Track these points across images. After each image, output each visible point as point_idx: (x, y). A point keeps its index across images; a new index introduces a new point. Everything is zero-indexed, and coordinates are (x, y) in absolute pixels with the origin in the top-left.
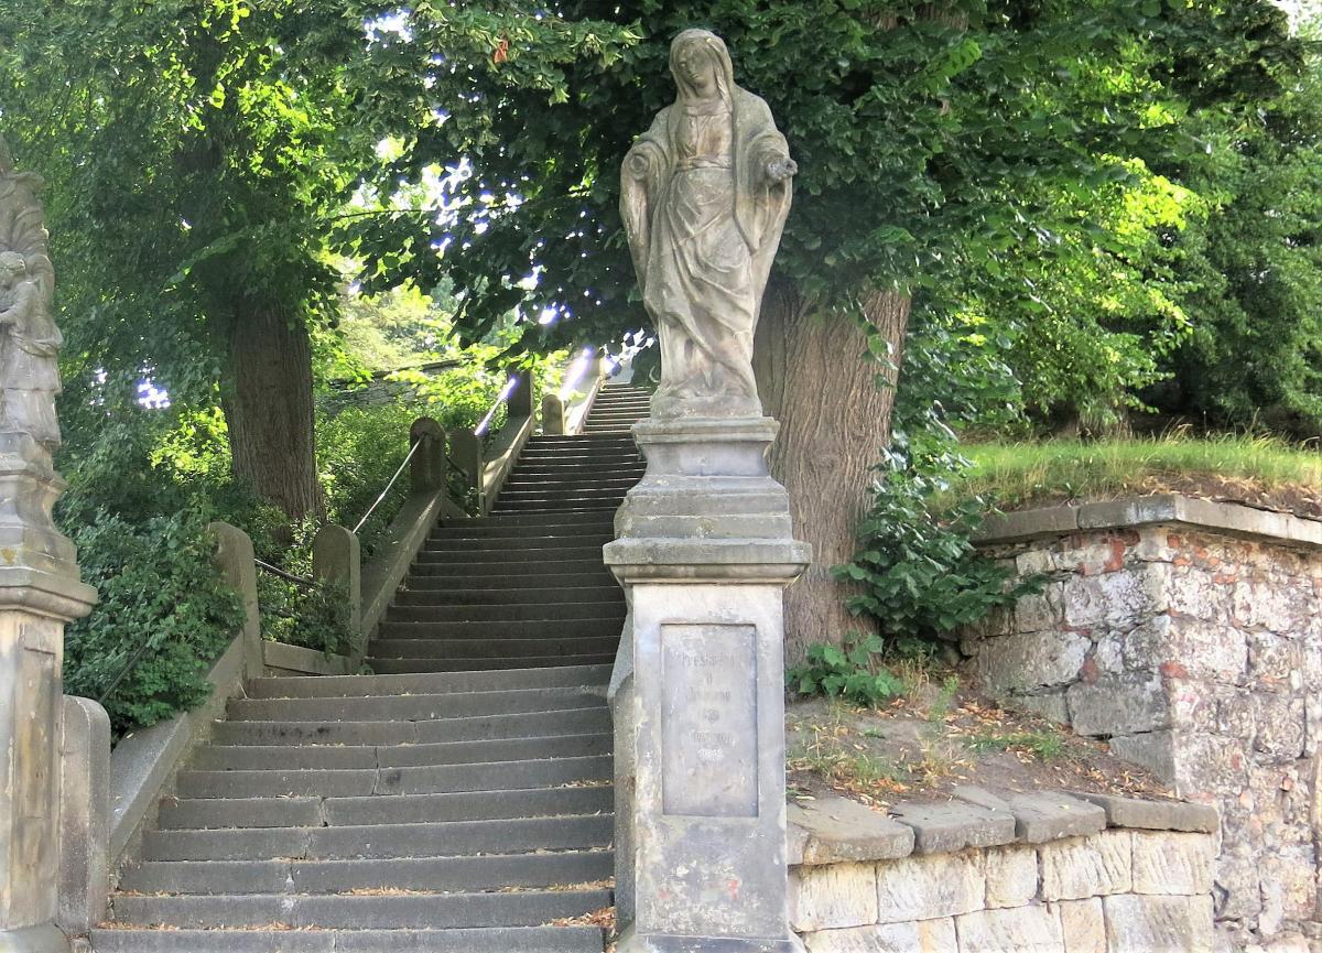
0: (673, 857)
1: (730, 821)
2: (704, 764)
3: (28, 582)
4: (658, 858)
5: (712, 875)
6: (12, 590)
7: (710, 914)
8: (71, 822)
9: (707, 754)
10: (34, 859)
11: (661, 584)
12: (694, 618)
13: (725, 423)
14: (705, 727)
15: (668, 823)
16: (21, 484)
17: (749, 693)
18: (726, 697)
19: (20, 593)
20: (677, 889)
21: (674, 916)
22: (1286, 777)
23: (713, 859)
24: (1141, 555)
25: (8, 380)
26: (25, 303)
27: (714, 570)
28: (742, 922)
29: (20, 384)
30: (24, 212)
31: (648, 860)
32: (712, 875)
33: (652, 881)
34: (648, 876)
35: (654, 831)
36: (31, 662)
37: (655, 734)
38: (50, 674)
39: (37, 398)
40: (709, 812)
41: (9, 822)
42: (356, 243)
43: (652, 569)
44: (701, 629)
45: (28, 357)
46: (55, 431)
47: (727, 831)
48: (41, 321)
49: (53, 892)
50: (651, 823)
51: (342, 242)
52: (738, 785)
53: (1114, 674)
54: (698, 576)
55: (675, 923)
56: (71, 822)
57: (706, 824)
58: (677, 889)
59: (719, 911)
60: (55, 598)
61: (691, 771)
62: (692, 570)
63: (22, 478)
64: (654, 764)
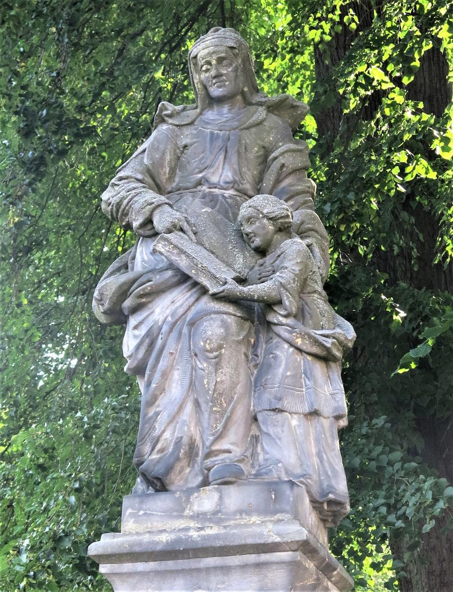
16: (295, 567)
25: (267, 396)
26: (297, 269)
29: (286, 404)
30: (280, 150)
39: (312, 428)
42: (387, 16)
45: (299, 357)
48: (320, 303)
63: (299, 556)
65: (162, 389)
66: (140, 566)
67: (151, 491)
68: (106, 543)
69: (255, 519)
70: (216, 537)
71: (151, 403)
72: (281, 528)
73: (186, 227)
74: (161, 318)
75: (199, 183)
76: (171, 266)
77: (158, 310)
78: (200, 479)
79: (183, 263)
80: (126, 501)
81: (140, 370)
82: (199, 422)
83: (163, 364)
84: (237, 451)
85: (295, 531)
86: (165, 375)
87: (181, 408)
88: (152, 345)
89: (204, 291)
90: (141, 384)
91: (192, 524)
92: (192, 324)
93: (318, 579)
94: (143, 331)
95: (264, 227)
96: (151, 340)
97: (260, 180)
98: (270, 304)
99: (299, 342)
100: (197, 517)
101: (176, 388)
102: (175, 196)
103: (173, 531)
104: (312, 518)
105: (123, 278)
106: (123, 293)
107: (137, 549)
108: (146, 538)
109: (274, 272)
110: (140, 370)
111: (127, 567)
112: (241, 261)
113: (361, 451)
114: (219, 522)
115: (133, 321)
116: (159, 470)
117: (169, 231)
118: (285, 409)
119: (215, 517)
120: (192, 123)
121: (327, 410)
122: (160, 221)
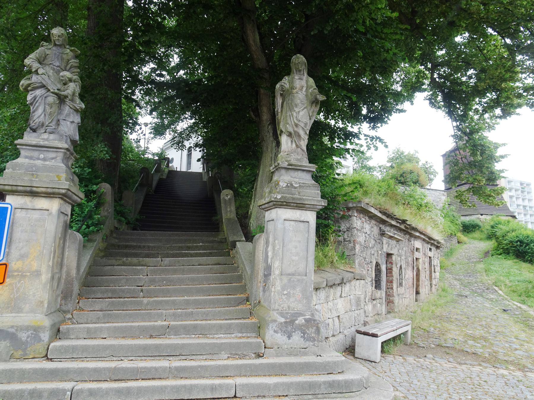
0: (283, 289)
1: (299, 277)
2: (293, 261)
3: (67, 188)
4: (279, 288)
5: (293, 293)
6: (60, 190)
7: (292, 305)
8: (68, 273)
9: (294, 258)
10: (56, 288)
11: (285, 208)
12: (293, 219)
13: (302, 164)
14: (294, 250)
15: (282, 278)
16: (65, 153)
18: (300, 242)
19: (64, 191)
21: (282, 306)
22: (368, 267)
23: (294, 288)
24: (350, 214)
27: (301, 205)
28: (301, 307)
31: (276, 289)
32: (293, 293)
33: (277, 295)
35: (278, 280)
36: (62, 216)
37: (280, 251)
38: (65, 222)
40: (293, 275)
41: (50, 275)
43: (285, 203)
44: (294, 222)
45: (70, 109)
46: (77, 138)
47: (298, 280)
49: (59, 299)
50: (278, 278)
52: (301, 267)
54: (296, 207)
55: (283, 308)
56: (68, 273)
58: (284, 297)
59: (295, 304)
60: (74, 196)
61: (289, 263)
62: (295, 205)
63: (65, 151)
64: (280, 260)
65: (36, 110)
66: (28, 147)
67: (31, 131)
68: (19, 141)
69: (56, 142)
70: (47, 144)
71: (34, 112)
72: (62, 144)
73: (46, 74)
74: (38, 94)
75: (51, 64)
76: (41, 83)
77: (37, 92)
78: (44, 131)
79: (44, 83)
80: (25, 132)
81: (31, 104)
82: (45, 119)
83: (37, 104)
84: (54, 127)
85: (66, 146)
86: (38, 107)
87: (41, 115)
88: (35, 99)
89: (49, 90)
90: (31, 108)
91: (41, 140)
92: (46, 97)
93: (70, 156)
94: (33, 96)
95: (66, 79)
96: (35, 98)
97: (66, 67)
98: (66, 97)
99: (71, 106)
100: (43, 139)
101: (40, 111)
102: (44, 65)
103: (37, 141)
104: (70, 143)
105: (28, 82)
106: (29, 85)
107: (27, 144)
108: (30, 142)
109: (67, 90)
110: (31, 104)
111: (24, 147)
112: (59, 86)
113: (84, 153)
114: (48, 141)
115: (30, 93)
116: (34, 127)
117: (42, 74)
118: (72, 387)
119: (47, 140)
120: (50, 49)
121: (76, 121)
122: (40, 71)
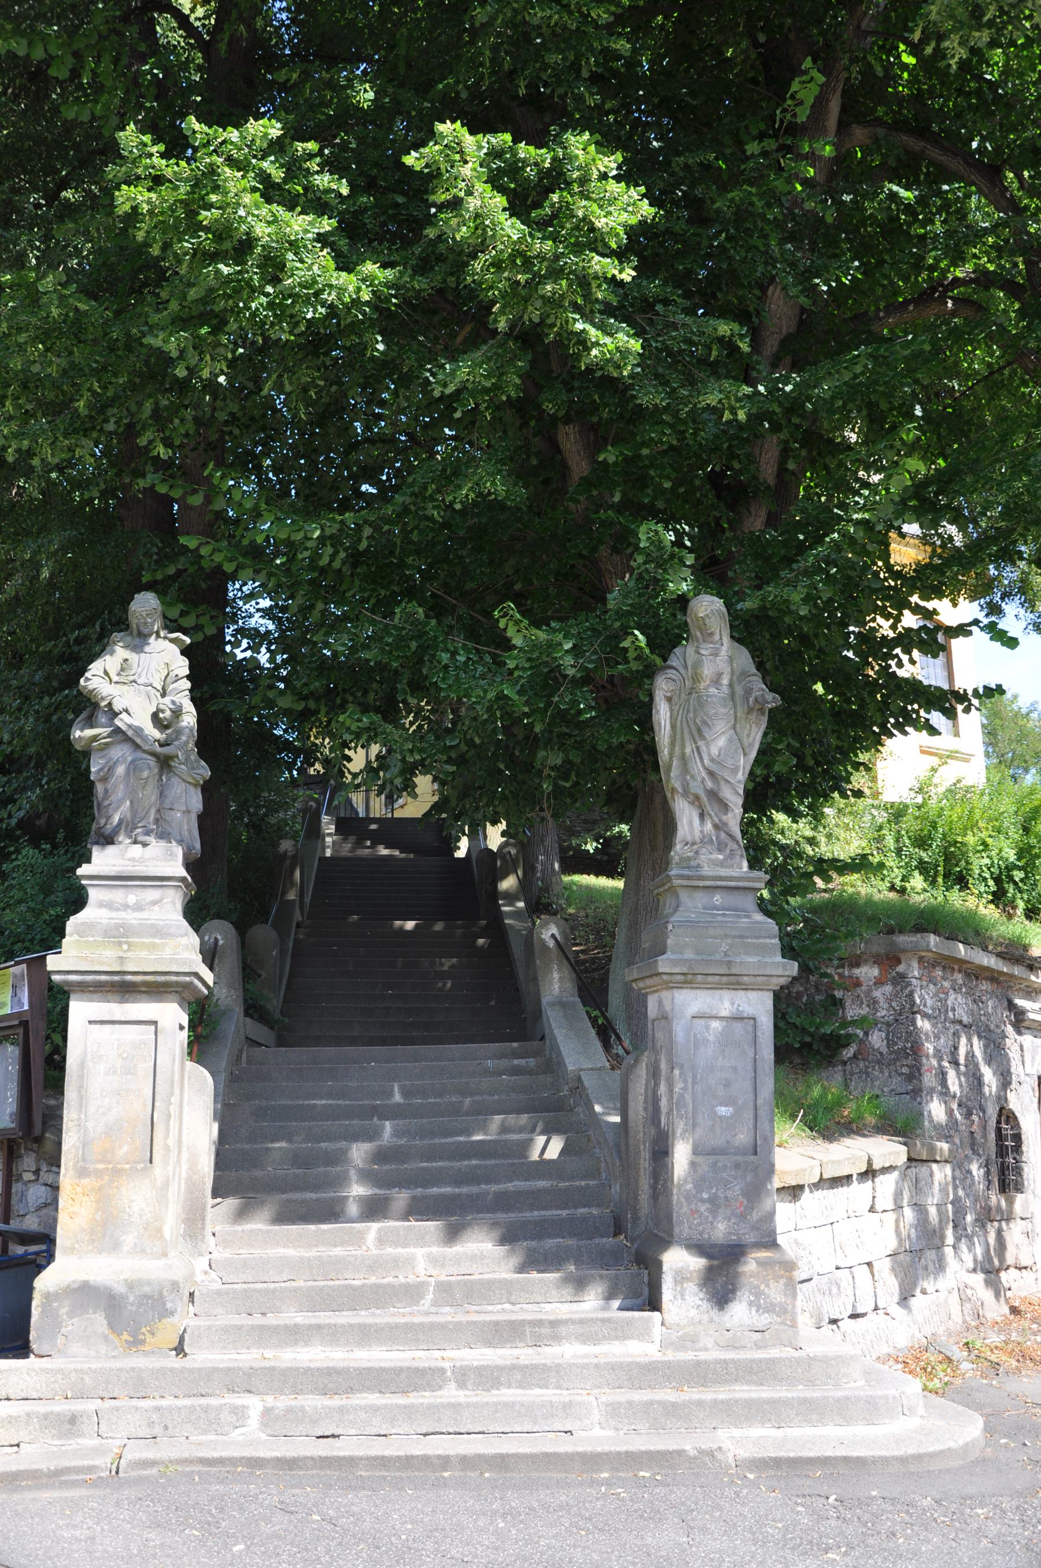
17: (750, 1067)
20: (703, 1208)
29: (175, 806)
32: (726, 1197)
34: (683, 1200)
51: (35, 553)
53: (881, 1053)
55: (701, 1234)
57: (723, 1161)
58: (703, 1208)
